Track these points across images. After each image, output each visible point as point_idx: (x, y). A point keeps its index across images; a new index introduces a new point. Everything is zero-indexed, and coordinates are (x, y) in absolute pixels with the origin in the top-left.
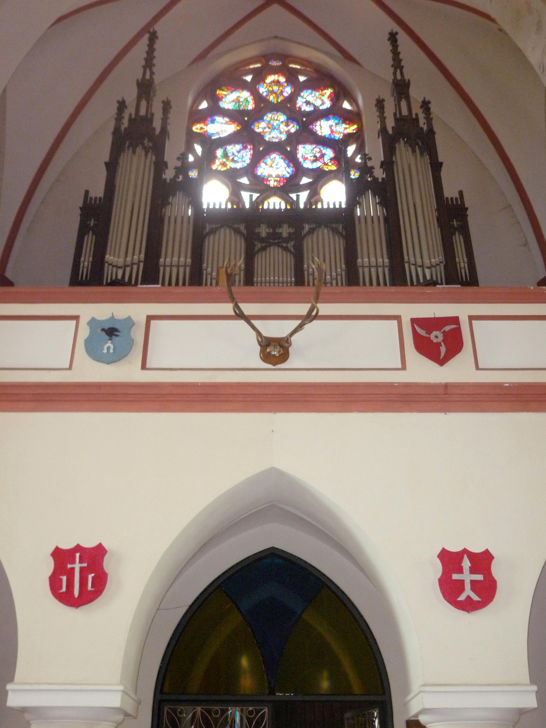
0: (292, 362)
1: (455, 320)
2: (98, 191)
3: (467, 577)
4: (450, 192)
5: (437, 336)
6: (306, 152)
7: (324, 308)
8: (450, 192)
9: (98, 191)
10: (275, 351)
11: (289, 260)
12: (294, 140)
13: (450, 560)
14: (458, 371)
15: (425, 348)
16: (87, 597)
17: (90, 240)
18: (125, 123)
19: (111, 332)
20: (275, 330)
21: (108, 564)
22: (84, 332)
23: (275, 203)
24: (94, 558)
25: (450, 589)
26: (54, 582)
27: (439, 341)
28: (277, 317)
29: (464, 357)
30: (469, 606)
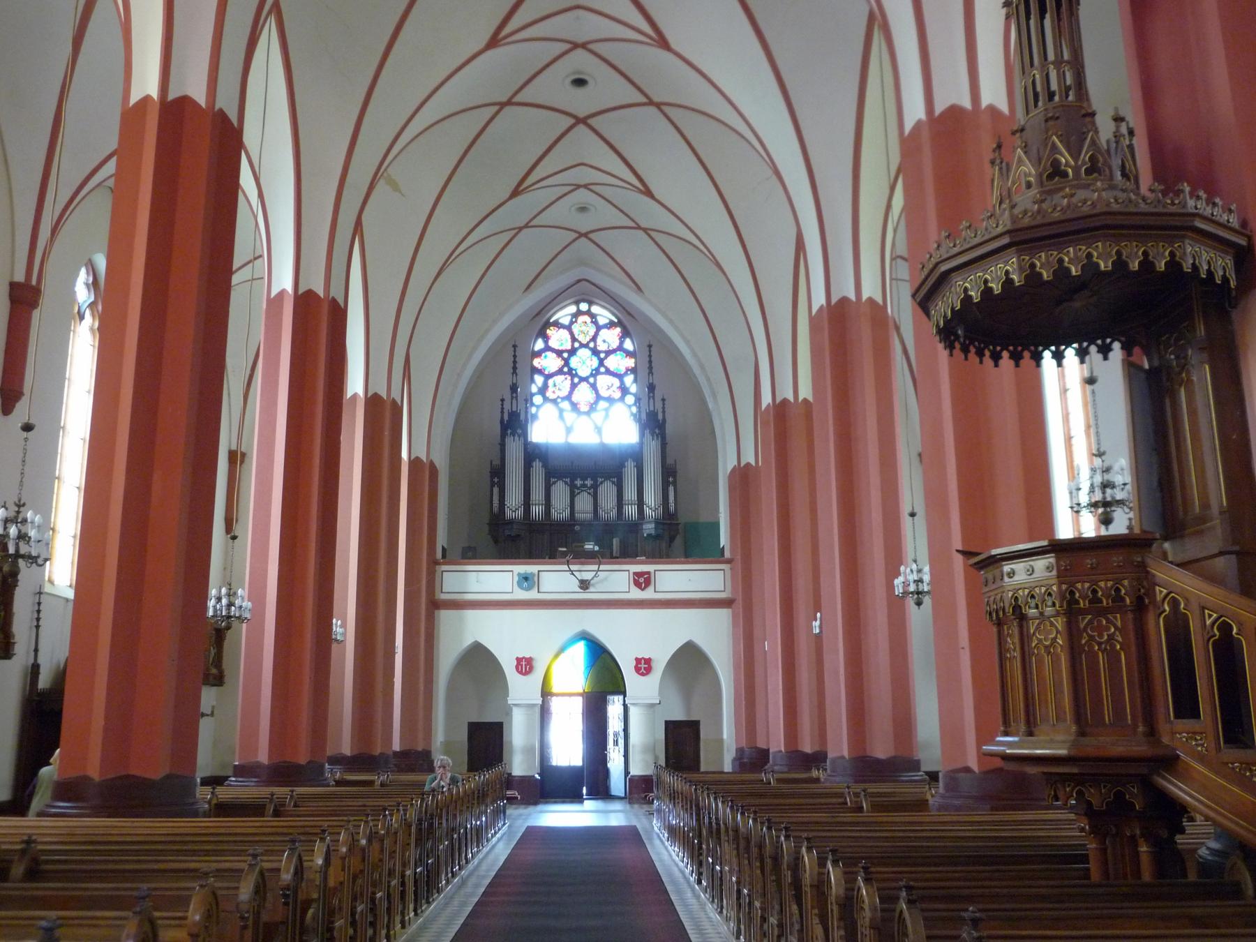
0: (592, 589)
1: (648, 573)
2: (497, 462)
3: (643, 666)
4: (670, 461)
5: (642, 580)
6: (603, 381)
7: (602, 567)
8: (670, 461)
9: (497, 462)
10: (584, 585)
11: (591, 499)
12: (595, 373)
13: (638, 661)
14: (648, 594)
15: (637, 584)
16: (526, 673)
17: (496, 490)
18: (506, 417)
19: (526, 579)
20: (587, 576)
21: (534, 664)
22: (516, 579)
23: (584, 307)
24: (529, 661)
25: (637, 669)
26: (517, 668)
27: (643, 581)
28: (587, 571)
29: (651, 588)
30: (642, 674)
